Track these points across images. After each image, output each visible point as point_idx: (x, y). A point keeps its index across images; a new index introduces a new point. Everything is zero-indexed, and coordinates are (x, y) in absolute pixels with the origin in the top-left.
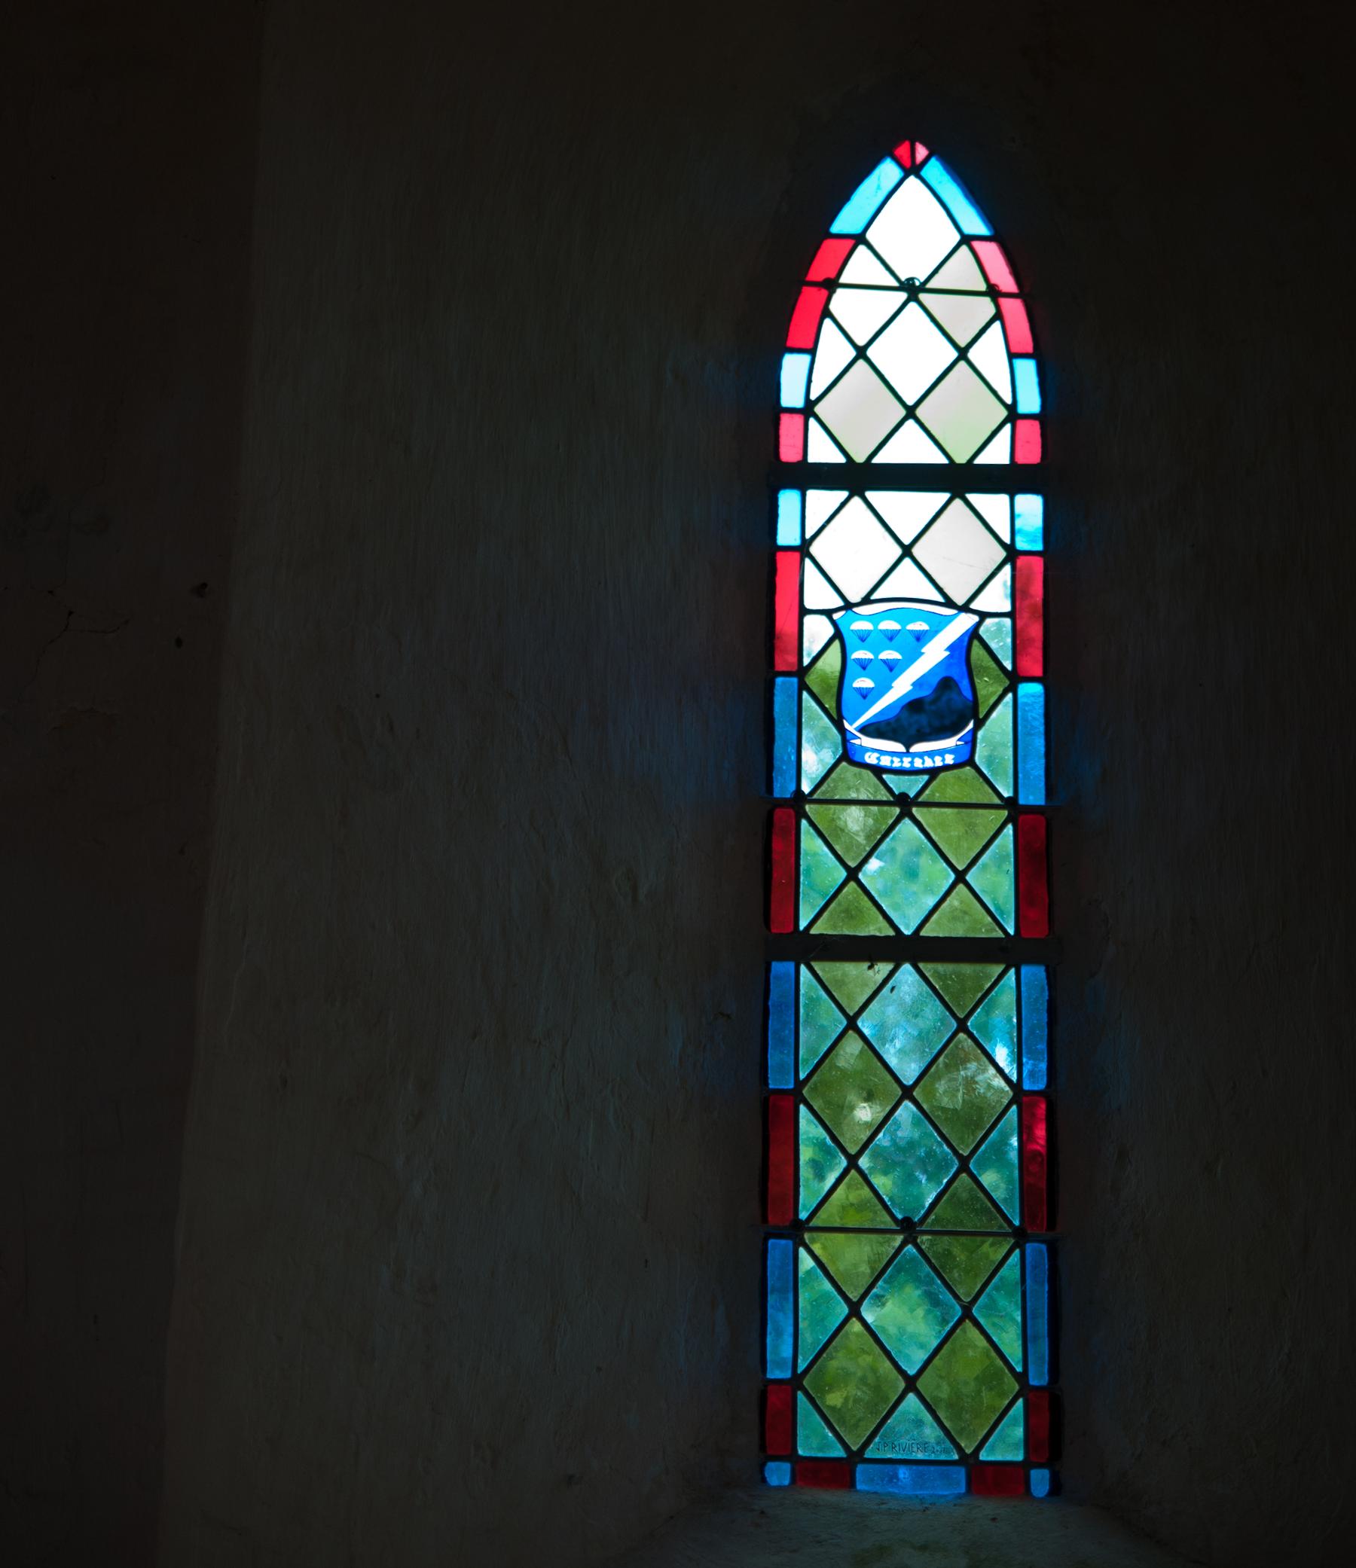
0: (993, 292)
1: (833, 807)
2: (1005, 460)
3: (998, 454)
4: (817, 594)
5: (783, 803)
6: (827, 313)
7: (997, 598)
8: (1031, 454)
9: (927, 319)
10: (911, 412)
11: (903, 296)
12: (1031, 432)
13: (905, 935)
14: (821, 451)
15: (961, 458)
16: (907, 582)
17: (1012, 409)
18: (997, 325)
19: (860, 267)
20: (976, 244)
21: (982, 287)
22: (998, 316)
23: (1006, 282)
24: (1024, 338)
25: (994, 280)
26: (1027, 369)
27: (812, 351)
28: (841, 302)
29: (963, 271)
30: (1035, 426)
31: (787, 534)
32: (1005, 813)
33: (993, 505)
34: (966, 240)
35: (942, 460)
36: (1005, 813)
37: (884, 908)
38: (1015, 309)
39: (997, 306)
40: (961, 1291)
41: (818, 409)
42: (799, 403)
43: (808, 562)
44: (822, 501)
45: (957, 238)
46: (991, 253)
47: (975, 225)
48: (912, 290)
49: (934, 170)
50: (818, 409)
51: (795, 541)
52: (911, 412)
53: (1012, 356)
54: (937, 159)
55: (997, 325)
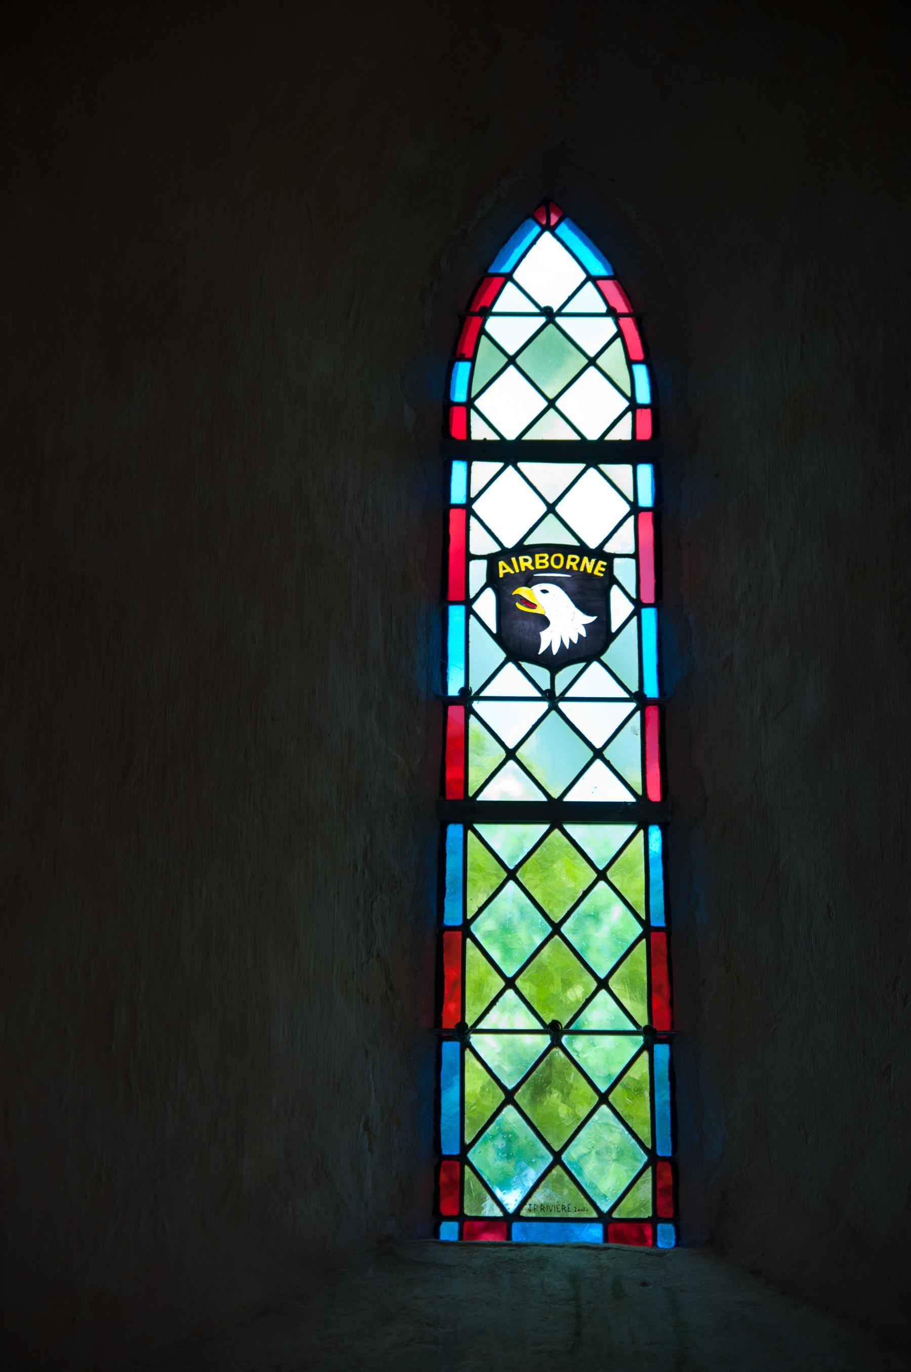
0: (611, 312)
1: (467, 1099)
2: (627, 436)
3: (623, 432)
4: (480, 544)
5: (454, 701)
6: (483, 332)
7: (624, 542)
8: (645, 433)
9: (570, 294)
10: (511, 754)
11: (542, 320)
12: (645, 417)
13: (463, 1212)
14: (479, 432)
15: (593, 435)
16: (551, 533)
17: (632, 399)
18: (618, 341)
19: (509, 299)
20: (600, 283)
21: (603, 309)
22: (619, 334)
23: (622, 307)
24: (637, 352)
25: (612, 304)
26: (641, 371)
27: (473, 360)
28: (492, 325)
29: (591, 300)
30: (648, 412)
31: (457, 496)
32: (633, 705)
33: (621, 472)
34: (590, 278)
35: (575, 437)
36: (633, 705)
37: (480, 1129)
38: (628, 324)
39: (617, 324)
40: (556, 1145)
41: (477, 403)
42: (459, 922)
43: (473, 412)
44: (483, 470)
45: (583, 276)
46: (610, 287)
47: (598, 268)
48: (549, 314)
49: (564, 230)
50: (477, 403)
51: (456, 1151)
52: (511, 754)
53: (630, 363)
54: (568, 225)
55: (618, 341)
